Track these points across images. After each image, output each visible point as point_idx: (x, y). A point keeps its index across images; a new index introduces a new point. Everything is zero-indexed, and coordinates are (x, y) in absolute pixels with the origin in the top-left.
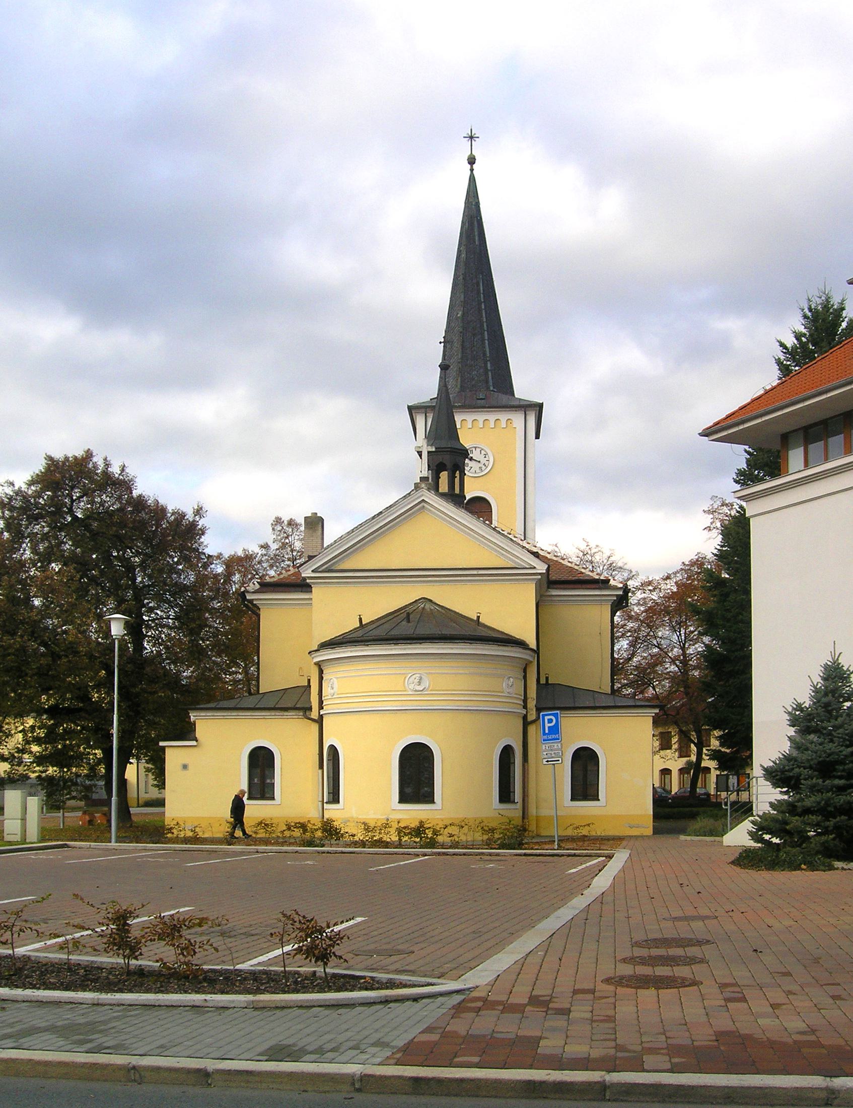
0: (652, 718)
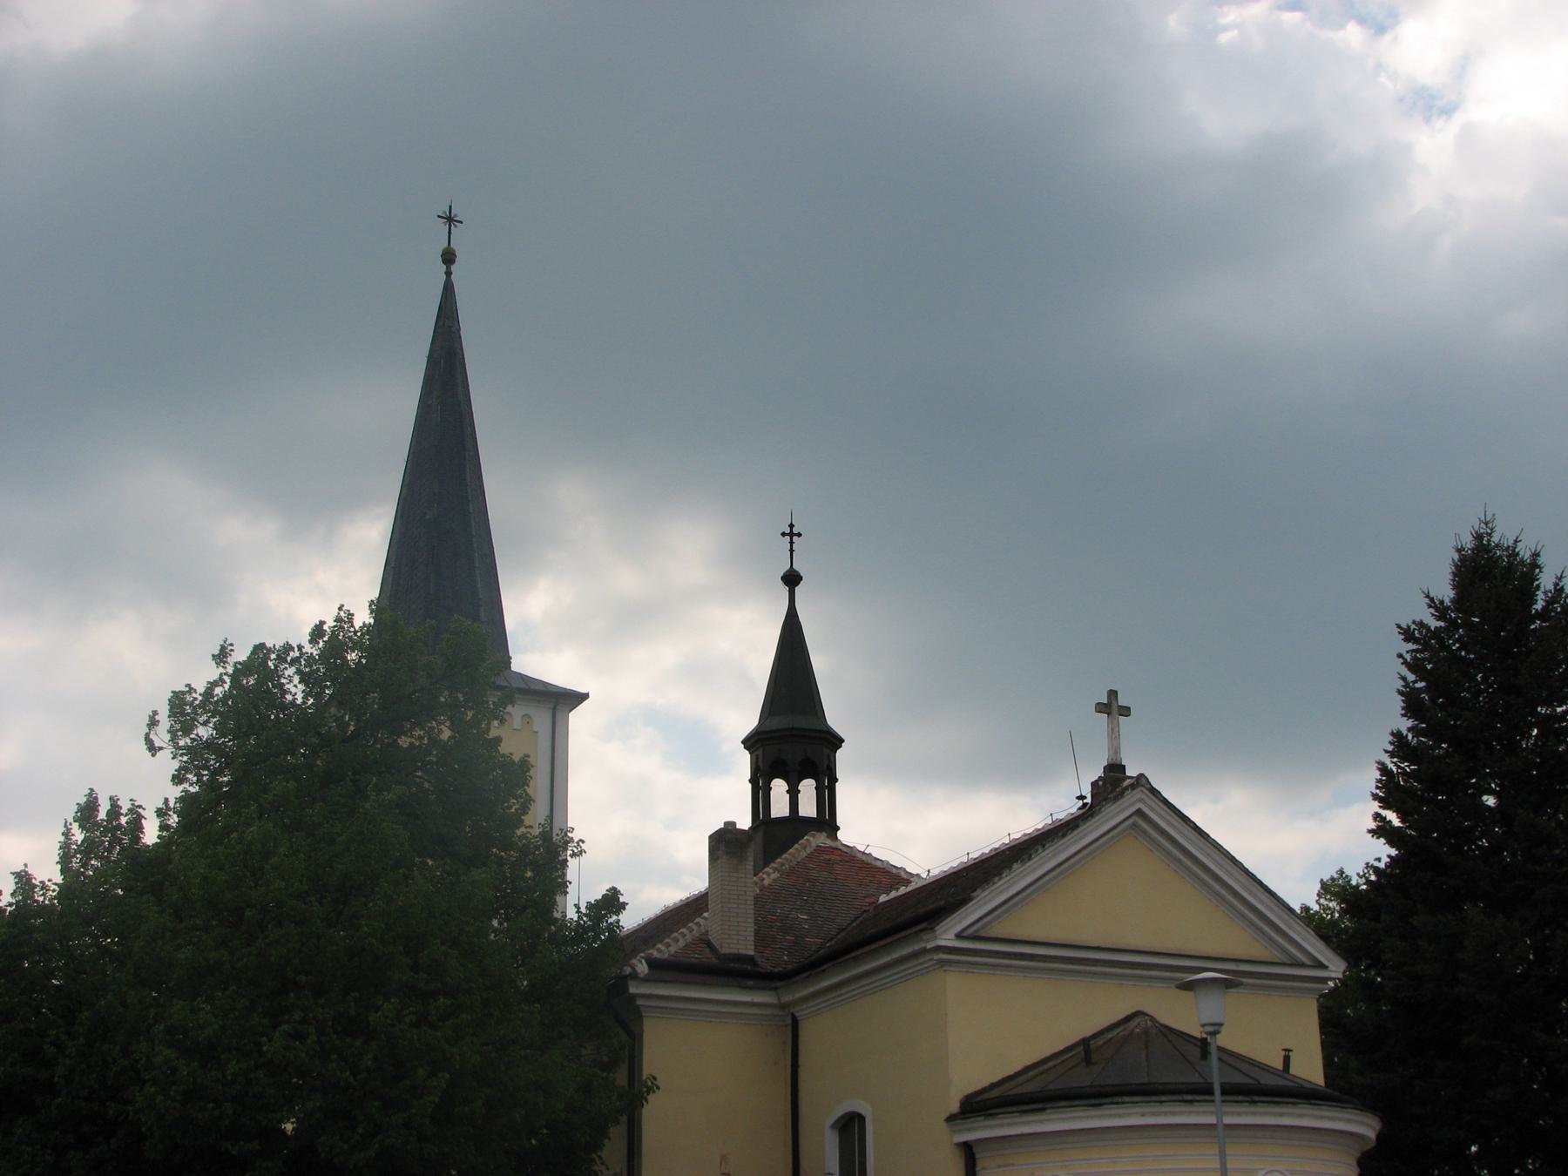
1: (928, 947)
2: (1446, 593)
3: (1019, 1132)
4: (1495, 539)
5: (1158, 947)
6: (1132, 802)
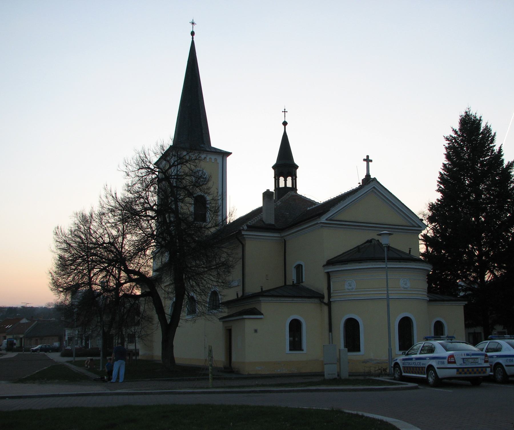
0: (463, 306)
1: (319, 222)
2: (457, 127)
3: (341, 269)
4: (471, 113)
5: (377, 222)
6: (372, 185)
